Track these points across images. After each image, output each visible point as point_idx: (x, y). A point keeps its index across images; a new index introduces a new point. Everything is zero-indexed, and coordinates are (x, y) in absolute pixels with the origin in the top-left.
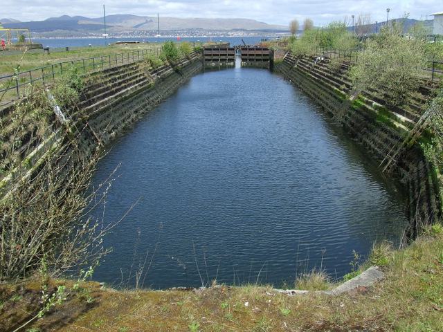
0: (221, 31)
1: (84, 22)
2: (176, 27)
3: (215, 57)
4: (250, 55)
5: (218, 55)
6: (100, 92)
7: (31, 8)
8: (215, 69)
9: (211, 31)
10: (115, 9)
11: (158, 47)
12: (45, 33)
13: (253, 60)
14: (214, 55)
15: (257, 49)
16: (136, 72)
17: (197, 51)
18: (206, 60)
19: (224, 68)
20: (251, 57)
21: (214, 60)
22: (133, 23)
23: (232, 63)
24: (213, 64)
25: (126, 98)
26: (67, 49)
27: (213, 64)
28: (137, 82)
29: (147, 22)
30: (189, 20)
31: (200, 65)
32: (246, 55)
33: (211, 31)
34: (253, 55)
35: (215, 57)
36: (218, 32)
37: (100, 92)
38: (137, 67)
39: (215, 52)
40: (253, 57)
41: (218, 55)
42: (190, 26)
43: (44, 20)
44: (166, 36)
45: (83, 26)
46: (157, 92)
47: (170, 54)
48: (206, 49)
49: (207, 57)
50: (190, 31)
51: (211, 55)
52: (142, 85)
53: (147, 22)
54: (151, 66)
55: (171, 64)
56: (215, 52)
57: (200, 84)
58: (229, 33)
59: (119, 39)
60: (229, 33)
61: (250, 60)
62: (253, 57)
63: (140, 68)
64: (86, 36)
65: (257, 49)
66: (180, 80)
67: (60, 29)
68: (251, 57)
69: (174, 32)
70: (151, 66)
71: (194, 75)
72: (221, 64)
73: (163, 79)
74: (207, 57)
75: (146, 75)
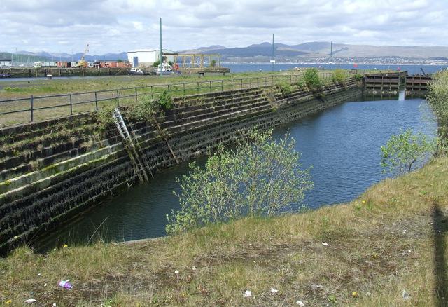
0: (417, 59)
1: (282, 49)
2: (370, 55)
3: (377, 86)
4: (415, 84)
5: (381, 83)
6: (198, 113)
7: (234, 36)
8: (377, 97)
9: (407, 59)
10: (310, 37)
11: (301, 73)
12: (247, 58)
13: (418, 89)
14: (376, 83)
15: (415, 78)
16: (256, 97)
17: (358, 79)
18: (368, 88)
19: (386, 97)
20: (416, 86)
21: (376, 88)
22: (325, 52)
23: (396, 92)
24: (375, 92)
25: (231, 121)
26: (72, 88)
27: (375, 92)
28: (253, 106)
29: (342, 49)
30: (384, 47)
31: (359, 92)
32: (411, 84)
33: (407, 59)
34: (418, 84)
35: (377, 86)
36: (415, 61)
37: (198, 113)
38: (262, 92)
39: (378, 80)
40: (419, 87)
41: (381, 83)
42: (386, 54)
43: (246, 46)
44: (360, 64)
45: (282, 52)
46: (278, 117)
47: (311, 80)
48: (369, 77)
49: (368, 85)
50: (385, 59)
51: (373, 83)
52: (261, 109)
53: (342, 49)
54: (282, 91)
55: (311, 90)
56: (378, 80)
57: (351, 112)
58: (427, 61)
59: (297, 65)
60: (427, 61)
61: (414, 89)
62: (419, 87)
63: (264, 93)
64: (283, 62)
65: (415, 78)
66: (318, 106)
67: (260, 54)
68: (416, 86)
69: (369, 59)
70: (282, 91)
71: (351, 100)
72: (383, 92)
73: (294, 105)
74: (368, 85)
75: (269, 100)
